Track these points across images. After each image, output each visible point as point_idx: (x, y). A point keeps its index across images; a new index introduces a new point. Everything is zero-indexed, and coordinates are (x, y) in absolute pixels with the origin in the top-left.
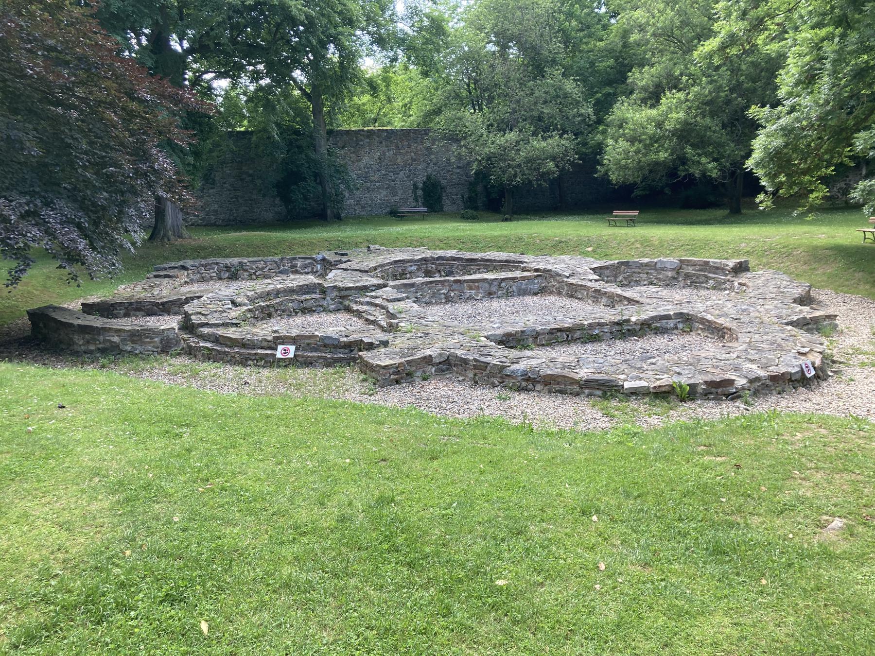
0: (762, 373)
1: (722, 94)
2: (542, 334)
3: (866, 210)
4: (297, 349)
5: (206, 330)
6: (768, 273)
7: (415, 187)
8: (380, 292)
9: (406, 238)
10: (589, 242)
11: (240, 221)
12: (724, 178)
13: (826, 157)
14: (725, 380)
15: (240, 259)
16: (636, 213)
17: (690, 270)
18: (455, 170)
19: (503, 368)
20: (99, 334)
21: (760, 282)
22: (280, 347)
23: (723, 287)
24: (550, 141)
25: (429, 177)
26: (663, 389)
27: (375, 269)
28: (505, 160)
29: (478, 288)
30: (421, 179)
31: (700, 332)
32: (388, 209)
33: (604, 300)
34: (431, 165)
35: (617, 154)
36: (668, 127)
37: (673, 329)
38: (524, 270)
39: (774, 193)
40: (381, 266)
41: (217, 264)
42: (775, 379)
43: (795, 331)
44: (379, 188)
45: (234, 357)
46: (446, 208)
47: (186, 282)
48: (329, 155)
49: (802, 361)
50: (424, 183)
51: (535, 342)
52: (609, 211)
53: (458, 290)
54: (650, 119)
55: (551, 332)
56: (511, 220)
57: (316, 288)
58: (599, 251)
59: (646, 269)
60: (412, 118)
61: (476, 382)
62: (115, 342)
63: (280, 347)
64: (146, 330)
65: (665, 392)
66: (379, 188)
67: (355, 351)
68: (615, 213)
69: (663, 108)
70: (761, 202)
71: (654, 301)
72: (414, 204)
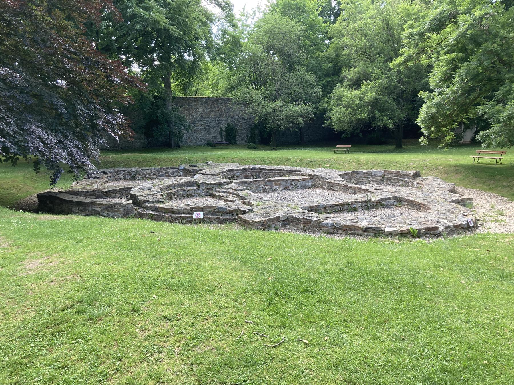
0: (450, 224)
1: (393, 84)
2: (328, 207)
3: (483, 145)
4: (204, 214)
5: (149, 205)
6: (431, 178)
7: (221, 130)
8: (229, 186)
9: (224, 158)
10: (327, 162)
11: (121, 148)
12: (395, 128)
13: (455, 118)
14: (434, 227)
15: (136, 169)
16: (350, 146)
17: (390, 176)
18: (243, 121)
19: (321, 222)
20: (89, 207)
21: (428, 182)
22: (195, 213)
23: (408, 185)
24: (299, 106)
25: (228, 125)
26: (405, 232)
27: (219, 174)
28: (275, 116)
29: (280, 184)
30: (224, 126)
31: (406, 206)
32: (206, 142)
33: (350, 191)
34: (230, 118)
35: (337, 115)
36: (366, 100)
37: (392, 205)
38: (302, 175)
39: (429, 137)
40: (222, 172)
41: (124, 171)
42: (456, 227)
43: (456, 205)
44: (201, 130)
45: (168, 219)
46: (238, 142)
47: (106, 181)
48: (174, 111)
49: (466, 219)
50: (226, 128)
51: (324, 211)
52: (335, 146)
53: (270, 186)
54: (356, 96)
55: (332, 206)
56: (276, 150)
57: (194, 183)
58: (333, 166)
59: (366, 176)
60: (219, 91)
61: (305, 230)
62: (98, 211)
63: (195, 213)
64: (116, 204)
65: (405, 233)
66: (201, 130)
67: (235, 215)
68: (338, 146)
69: (363, 90)
70: (422, 141)
71: (379, 192)
72: (220, 139)
